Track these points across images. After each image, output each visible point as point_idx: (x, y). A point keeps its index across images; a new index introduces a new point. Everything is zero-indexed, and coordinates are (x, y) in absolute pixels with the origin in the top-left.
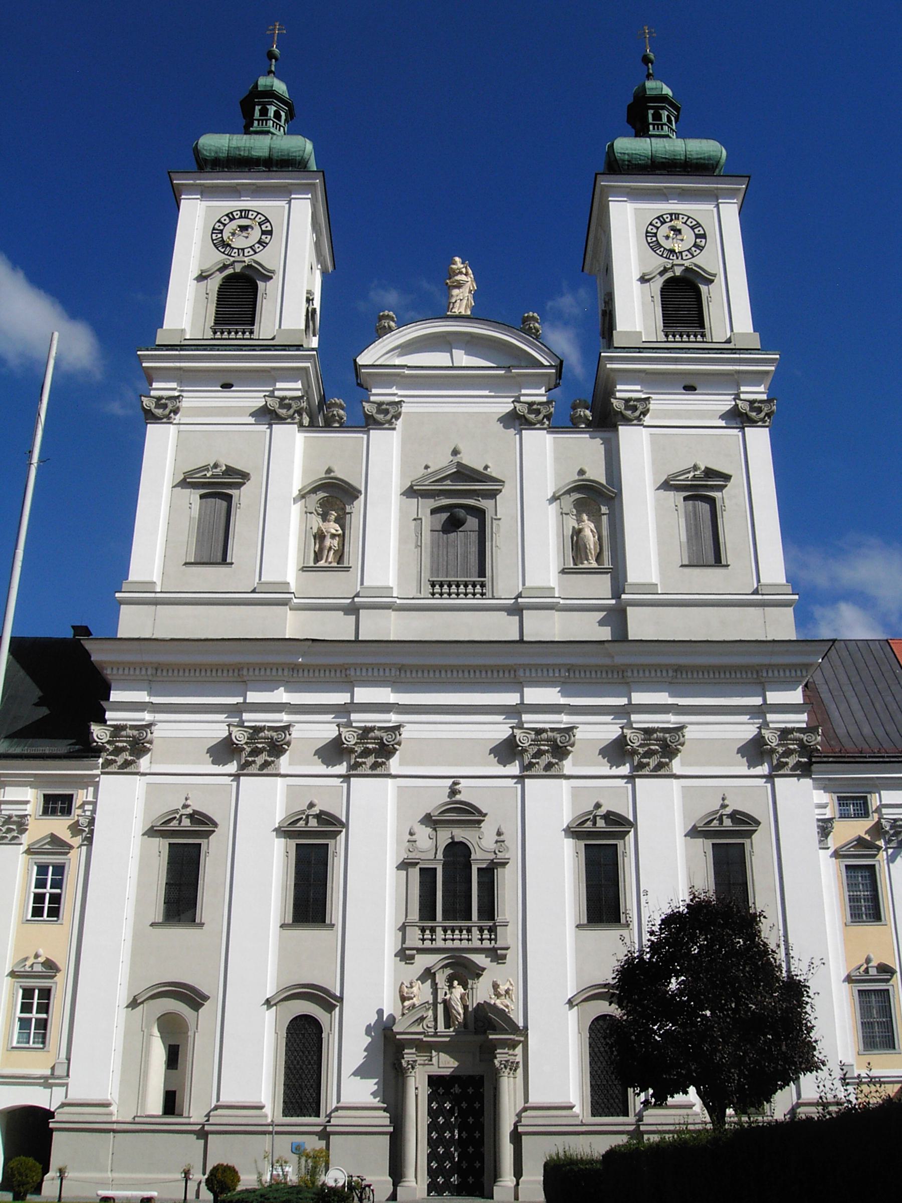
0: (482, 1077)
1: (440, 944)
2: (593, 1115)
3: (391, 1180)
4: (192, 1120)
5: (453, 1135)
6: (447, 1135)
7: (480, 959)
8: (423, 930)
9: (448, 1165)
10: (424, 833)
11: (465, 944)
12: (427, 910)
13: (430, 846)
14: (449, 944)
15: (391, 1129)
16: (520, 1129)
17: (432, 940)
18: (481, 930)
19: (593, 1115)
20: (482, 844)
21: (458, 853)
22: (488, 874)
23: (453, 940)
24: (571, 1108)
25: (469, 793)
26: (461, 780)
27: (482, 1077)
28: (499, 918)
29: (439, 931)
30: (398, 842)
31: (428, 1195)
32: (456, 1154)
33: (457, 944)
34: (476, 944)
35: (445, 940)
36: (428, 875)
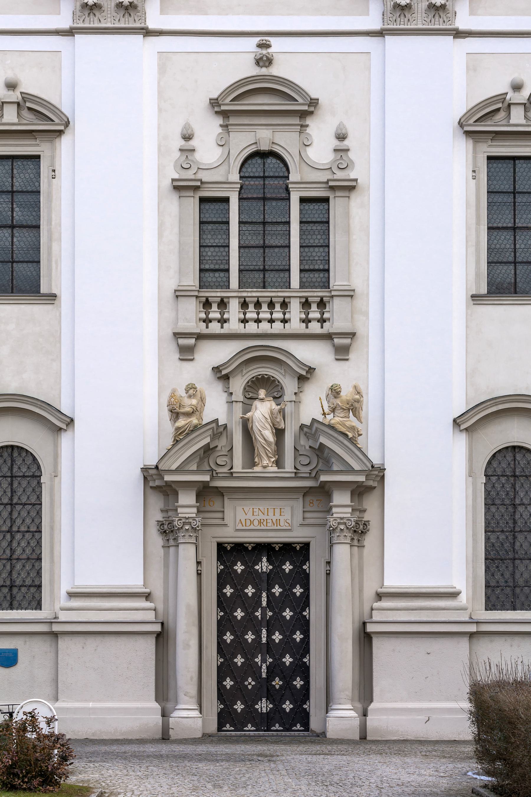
0: (306, 546)
1: (234, 326)
2: (488, 608)
3: (159, 707)
4: (286, 470)
5: (269, 636)
6: (250, 637)
7: (307, 353)
8: (207, 304)
9: (250, 683)
10: (208, 131)
11: (278, 327)
12: (211, 270)
13: (218, 157)
14: (252, 328)
15: (157, 628)
16: (370, 628)
17: (285, 321)
18: (306, 304)
19: (488, 608)
20: (312, 154)
21: (264, 170)
22: (317, 205)
23: (258, 321)
24: (454, 595)
25: (293, 64)
26: (273, 40)
27: (306, 546)
28: (337, 281)
29: (234, 306)
30: (162, 152)
31: (219, 729)
32: (264, 667)
33: (265, 327)
34: (295, 325)
35: (244, 321)
36: (212, 205)
